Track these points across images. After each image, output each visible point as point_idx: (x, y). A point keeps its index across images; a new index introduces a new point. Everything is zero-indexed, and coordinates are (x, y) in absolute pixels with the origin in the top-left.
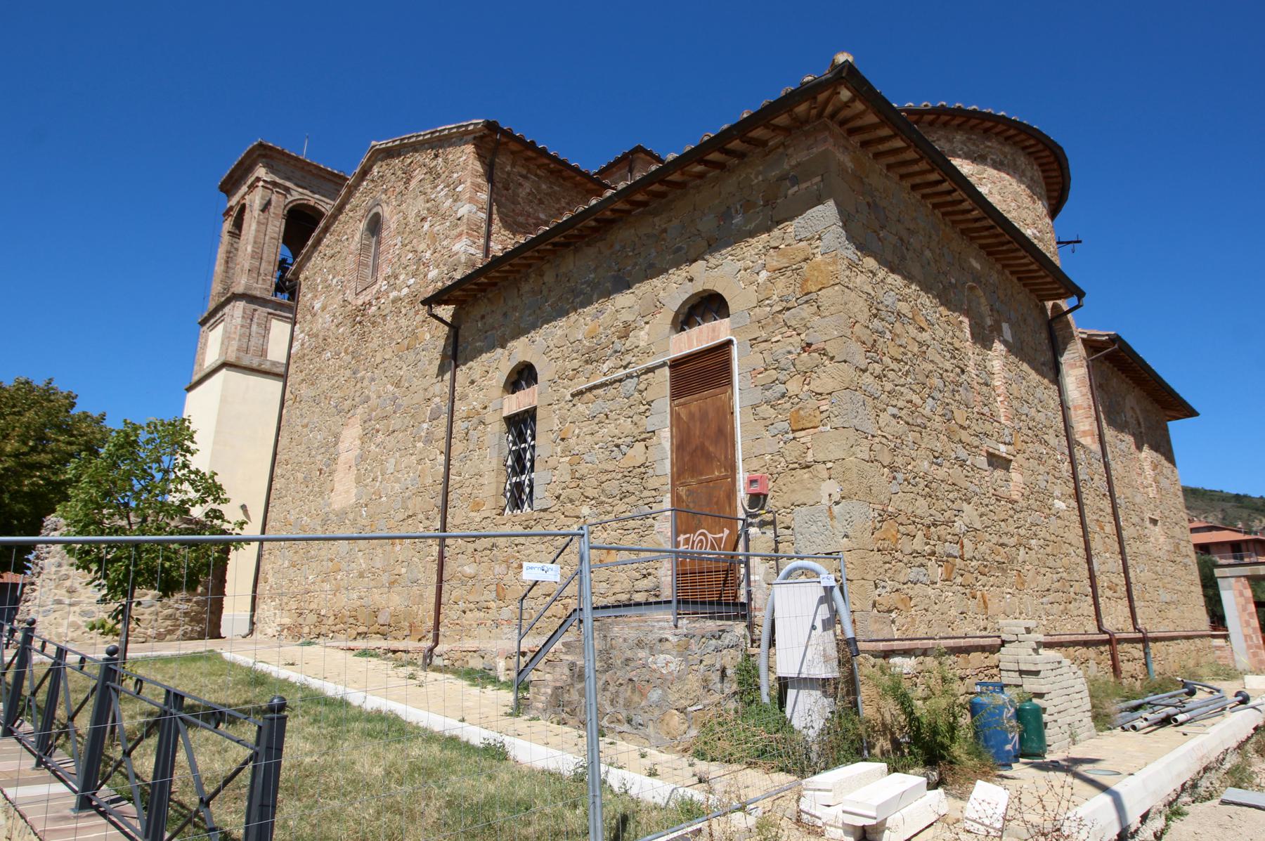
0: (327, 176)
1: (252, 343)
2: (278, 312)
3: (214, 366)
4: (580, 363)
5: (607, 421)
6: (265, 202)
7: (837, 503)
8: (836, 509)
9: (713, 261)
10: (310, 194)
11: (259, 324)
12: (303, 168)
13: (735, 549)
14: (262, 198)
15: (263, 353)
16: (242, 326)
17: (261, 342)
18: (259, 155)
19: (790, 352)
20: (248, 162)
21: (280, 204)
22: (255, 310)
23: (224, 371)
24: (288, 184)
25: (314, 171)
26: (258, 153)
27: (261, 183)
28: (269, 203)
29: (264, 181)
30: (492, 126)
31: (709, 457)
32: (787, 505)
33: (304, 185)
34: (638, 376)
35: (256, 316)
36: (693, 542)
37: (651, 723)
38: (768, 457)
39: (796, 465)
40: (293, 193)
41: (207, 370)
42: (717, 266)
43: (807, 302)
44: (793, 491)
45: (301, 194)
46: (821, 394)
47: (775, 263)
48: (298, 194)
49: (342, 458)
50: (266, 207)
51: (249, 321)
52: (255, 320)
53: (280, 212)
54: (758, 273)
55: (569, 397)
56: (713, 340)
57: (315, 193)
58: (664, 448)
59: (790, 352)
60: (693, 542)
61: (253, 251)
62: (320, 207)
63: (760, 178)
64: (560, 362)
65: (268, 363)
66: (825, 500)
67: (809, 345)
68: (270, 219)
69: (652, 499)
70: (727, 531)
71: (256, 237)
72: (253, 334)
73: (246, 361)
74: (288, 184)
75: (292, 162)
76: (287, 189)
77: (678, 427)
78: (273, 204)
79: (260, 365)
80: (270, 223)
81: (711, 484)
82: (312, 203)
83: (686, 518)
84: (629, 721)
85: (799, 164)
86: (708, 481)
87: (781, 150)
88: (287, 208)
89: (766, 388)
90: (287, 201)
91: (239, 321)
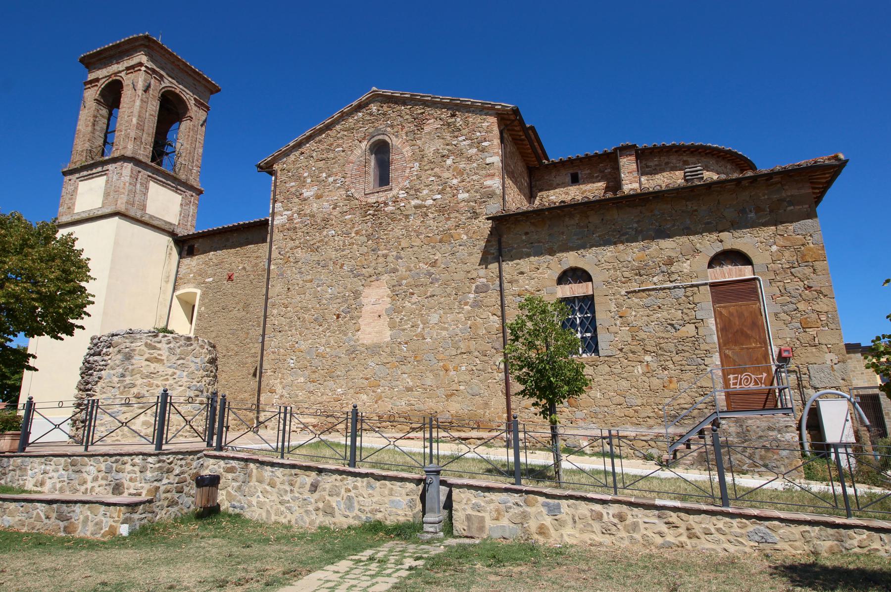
0: (190, 72)
1: (137, 199)
2: (155, 176)
3: (85, 216)
4: (632, 275)
5: (660, 310)
6: (147, 84)
7: (835, 364)
8: (835, 366)
9: (736, 234)
10: (176, 84)
11: (141, 184)
12: (173, 62)
13: (772, 384)
14: (145, 80)
15: (144, 207)
16: (130, 184)
17: (143, 198)
18: (142, 45)
19: (797, 289)
20: (126, 47)
21: (157, 88)
22: (139, 172)
23: (116, 218)
24: (162, 72)
25: (182, 66)
26: (142, 42)
27: (143, 68)
28: (149, 86)
29: (146, 67)
30: (516, 112)
31: (748, 337)
32: (803, 363)
33: (173, 76)
34: (685, 288)
35: (140, 177)
36: (741, 379)
37: (782, 466)
38: (788, 339)
39: (808, 345)
40: (166, 81)
41: (76, 217)
42: (740, 237)
43: (806, 266)
44: (807, 357)
45: (171, 82)
46: (821, 312)
47: (781, 243)
48: (168, 82)
49: (366, 309)
50: (147, 89)
51: (135, 180)
52: (139, 179)
53: (158, 95)
54: (770, 246)
55: (623, 293)
56: (740, 276)
57: (180, 84)
58: (712, 329)
59: (797, 289)
60: (741, 379)
61: (138, 123)
62: (183, 96)
63: (766, 197)
64: (612, 272)
65: (147, 216)
66: (829, 362)
67: (811, 287)
68: (150, 99)
69: (704, 355)
70: (765, 375)
71: (140, 112)
72: (138, 191)
73: (132, 213)
74: (162, 72)
75: (167, 56)
76: (162, 76)
77: (721, 318)
78: (152, 87)
79: (142, 217)
80: (150, 102)
81: (750, 350)
82: (177, 91)
83: (729, 366)
84: (766, 466)
85: (792, 196)
86: (748, 349)
87: (779, 185)
88: (161, 93)
89: (783, 305)
90: (162, 87)
91: (128, 179)
